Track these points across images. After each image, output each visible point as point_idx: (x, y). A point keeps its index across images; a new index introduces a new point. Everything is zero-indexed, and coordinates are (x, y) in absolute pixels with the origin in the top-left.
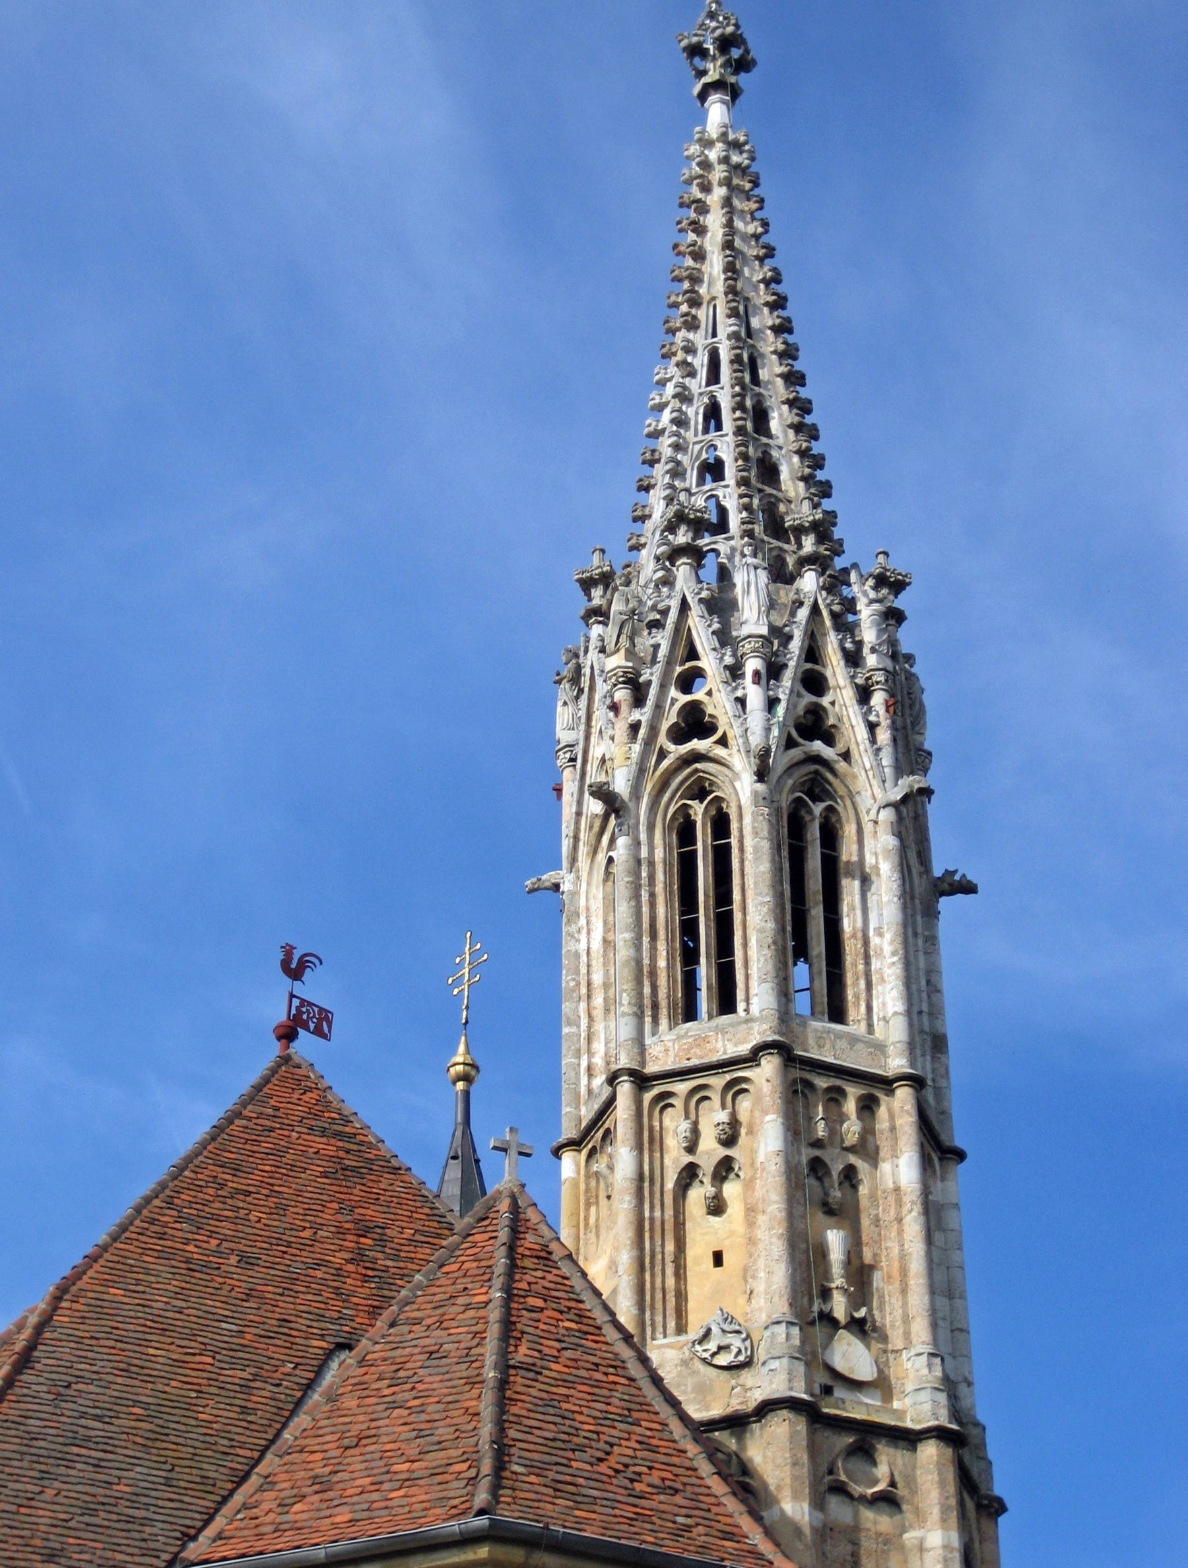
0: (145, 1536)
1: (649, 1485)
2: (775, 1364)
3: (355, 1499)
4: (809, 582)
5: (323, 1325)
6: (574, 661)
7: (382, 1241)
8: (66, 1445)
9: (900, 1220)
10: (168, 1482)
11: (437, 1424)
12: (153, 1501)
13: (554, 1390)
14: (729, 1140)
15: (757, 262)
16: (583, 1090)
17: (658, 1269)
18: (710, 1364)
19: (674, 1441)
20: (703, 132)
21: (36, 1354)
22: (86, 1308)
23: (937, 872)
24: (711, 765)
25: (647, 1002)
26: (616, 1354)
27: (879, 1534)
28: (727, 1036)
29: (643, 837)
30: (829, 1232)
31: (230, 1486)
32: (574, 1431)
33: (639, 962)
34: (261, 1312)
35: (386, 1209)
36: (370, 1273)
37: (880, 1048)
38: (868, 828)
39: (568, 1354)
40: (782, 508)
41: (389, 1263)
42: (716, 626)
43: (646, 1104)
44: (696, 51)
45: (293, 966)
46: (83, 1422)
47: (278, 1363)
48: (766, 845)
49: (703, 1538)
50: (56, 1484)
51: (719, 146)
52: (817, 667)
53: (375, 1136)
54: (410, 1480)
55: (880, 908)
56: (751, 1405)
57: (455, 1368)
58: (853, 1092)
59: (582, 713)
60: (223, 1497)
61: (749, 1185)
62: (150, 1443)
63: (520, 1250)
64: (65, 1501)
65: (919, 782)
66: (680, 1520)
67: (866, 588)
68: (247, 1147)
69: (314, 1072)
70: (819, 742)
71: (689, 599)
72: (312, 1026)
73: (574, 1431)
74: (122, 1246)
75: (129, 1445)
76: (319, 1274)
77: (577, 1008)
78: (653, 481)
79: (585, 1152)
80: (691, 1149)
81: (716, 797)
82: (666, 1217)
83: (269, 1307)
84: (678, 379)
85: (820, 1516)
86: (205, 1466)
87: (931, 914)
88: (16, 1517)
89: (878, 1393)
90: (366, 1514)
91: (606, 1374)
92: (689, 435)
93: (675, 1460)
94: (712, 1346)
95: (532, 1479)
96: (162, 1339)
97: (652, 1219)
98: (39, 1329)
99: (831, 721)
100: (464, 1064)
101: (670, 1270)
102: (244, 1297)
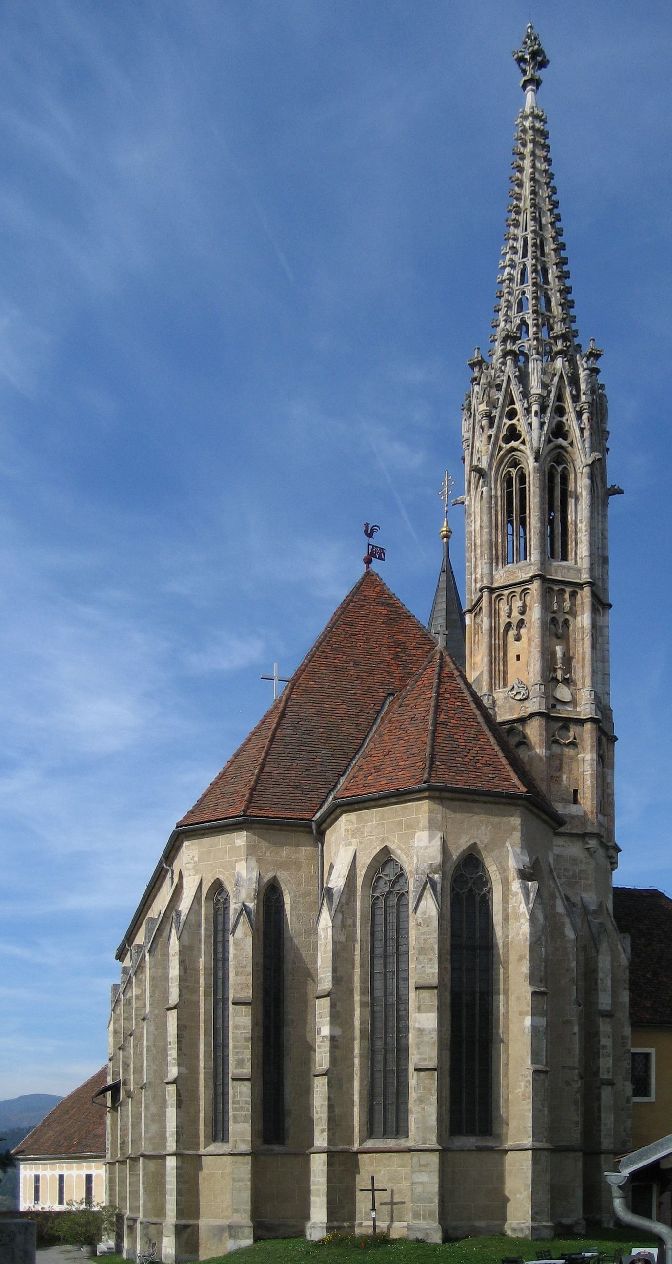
2: (535, 700)
3: (387, 775)
4: (559, 363)
7: (404, 649)
9: (583, 639)
10: (332, 756)
12: (328, 764)
13: (452, 731)
14: (522, 613)
17: (497, 663)
18: (514, 699)
19: (491, 746)
20: (524, 111)
21: (286, 711)
22: (302, 691)
23: (608, 486)
24: (519, 452)
25: (494, 557)
26: (474, 713)
27: (569, 756)
29: (493, 486)
30: (557, 647)
31: (353, 755)
32: (457, 746)
33: (491, 541)
35: (406, 635)
36: (400, 663)
37: (579, 571)
38: (579, 475)
41: (407, 658)
43: (493, 599)
45: (369, 532)
46: (303, 736)
48: (538, 490)
50: (296, 761)
51: (530, 119)
52: (561, 404)
53: (402, 603)
55: (582, 511)
56: (527, 715)
58: (568, 590)
59: (471, 426)
61: (529, 630)
62: (326, 742)
63: (443, 675)
64: (300, 767)
67: (583, 362)
68: (355, 615)
69: (378, 577)
70: (561, 439)
71: (511, 376)
72: (377, 556)
73: (457, 746)
74: (313, 664)
75: (319, 743)
76: (382, 666)
79: (474, 614)
80: (509, 617)
81: (521, 467)
87: (605, 504)
91: (470, 722)
92: (514, 285)
93: (491, 753)
94: (514, 692)
96: (328, 700)
98: (286, 702)
99: (566, 428)
100: (446, 531)
101: (501, 663)
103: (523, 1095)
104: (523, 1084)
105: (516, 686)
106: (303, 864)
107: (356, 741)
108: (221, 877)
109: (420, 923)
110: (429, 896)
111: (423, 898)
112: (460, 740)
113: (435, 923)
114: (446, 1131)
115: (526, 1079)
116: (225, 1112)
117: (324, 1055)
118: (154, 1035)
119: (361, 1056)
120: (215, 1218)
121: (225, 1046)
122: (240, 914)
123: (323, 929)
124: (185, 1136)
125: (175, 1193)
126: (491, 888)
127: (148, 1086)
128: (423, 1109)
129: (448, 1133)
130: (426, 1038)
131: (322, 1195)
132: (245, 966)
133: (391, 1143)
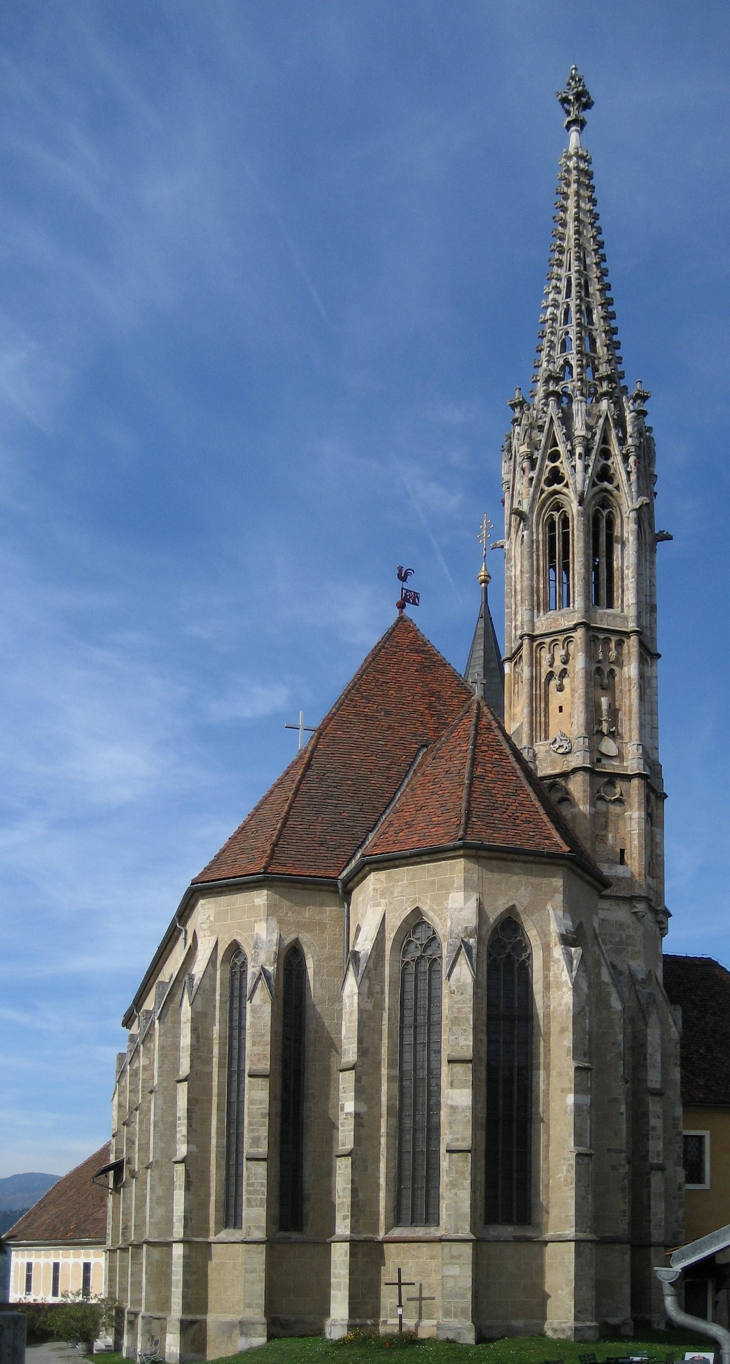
0: (354, 833)
1: (521, 821)
2: (578, 754)
3: (420, 832)
5: (416, 738)
6: (509, 441)
8: (324, 799)
9: (630, 691)
10: (361, 810)
11: (448, 802)
12: (356, 819)
14: (565, 662)
15: (590, 226)
16: (513, 636)
17: (538, 714)
18: (556, 752)
19: (532, 801)
20: (567, 151)
21: (312, 763)
22: (329, 741)
23: (657, 532)
24: (561, 495)
25: (535, 603)
27: (616, 814)
28: (565, 618)
29: (534, 530)
31: (383, 809)
32: (495, 802)
33: (532, 586)
34: (393, 735)
36: (434, 713)
37: (626, 619)
38: (625, 520)
39: (495, 769)
41: (442, 708)
42: (564, 431)
43: (534, 647)
45: (403, 575)
46: (330, 789)
47: (400, 756)
48: (582, 535)
49: (538, 840)
50: (322, 815)
51: (575, 159)
52: (607, 446)
53: (437, 651)
54: (437, 825)
55: (628, 557)
56: (570, 769)
57: (455, 778)
58: (614, 639)
59: (512, 468)
60: (381, 814)
61: (572, 680)
62: (354, 795)
63: (480, 726)
64: (325, 822)
65: (646, 500)
66: (530, 833)
67: (630, 404)
68: (387, 662)
71: (554, 417)
72: (411, 601)
73: (495, 802)
74: (341, 713)
75: (347, 797)
76: (415, 716)
77: (511, 601)
78: (543, 347)
79: (513, 663)
80: (551, 666)
82: (542, 693)
83: (396, 733)
85: (594, 809)
86: (374, 802)
87: (653, 550)
88: (309, 830)
89: (619, 760)
91: (509, 776)
92: (557, 326)
93: (531, 809)
94: (557, 746)
95: (479, 823)
97: (536, 694)
98: (312, 752)
99: (612, 472)
100: (485, 576)
101: (542, 715)
102: (387, 729)
103: (565, 1180)
104: (564, 1168)
105: (558, 739)
107: (386, 795)
108: (239, 939)
109: (454, 991)
110: (463, 962)
111: (457, 964)
112: (498, 796)
113: (470, 991)
114: (480, 1220)
115: (569, 1162)
116: (238, 1195)
117: (347, 1133)
121: (240, 1122)
122: (259, 979)
123: (348, 997)
125: (181, 1285)
126: (531, 954)
128: (456, 1194)
129: (482, 1222)
130: (459, 1117)
132: (263, 1036)
133: (420, 1232)
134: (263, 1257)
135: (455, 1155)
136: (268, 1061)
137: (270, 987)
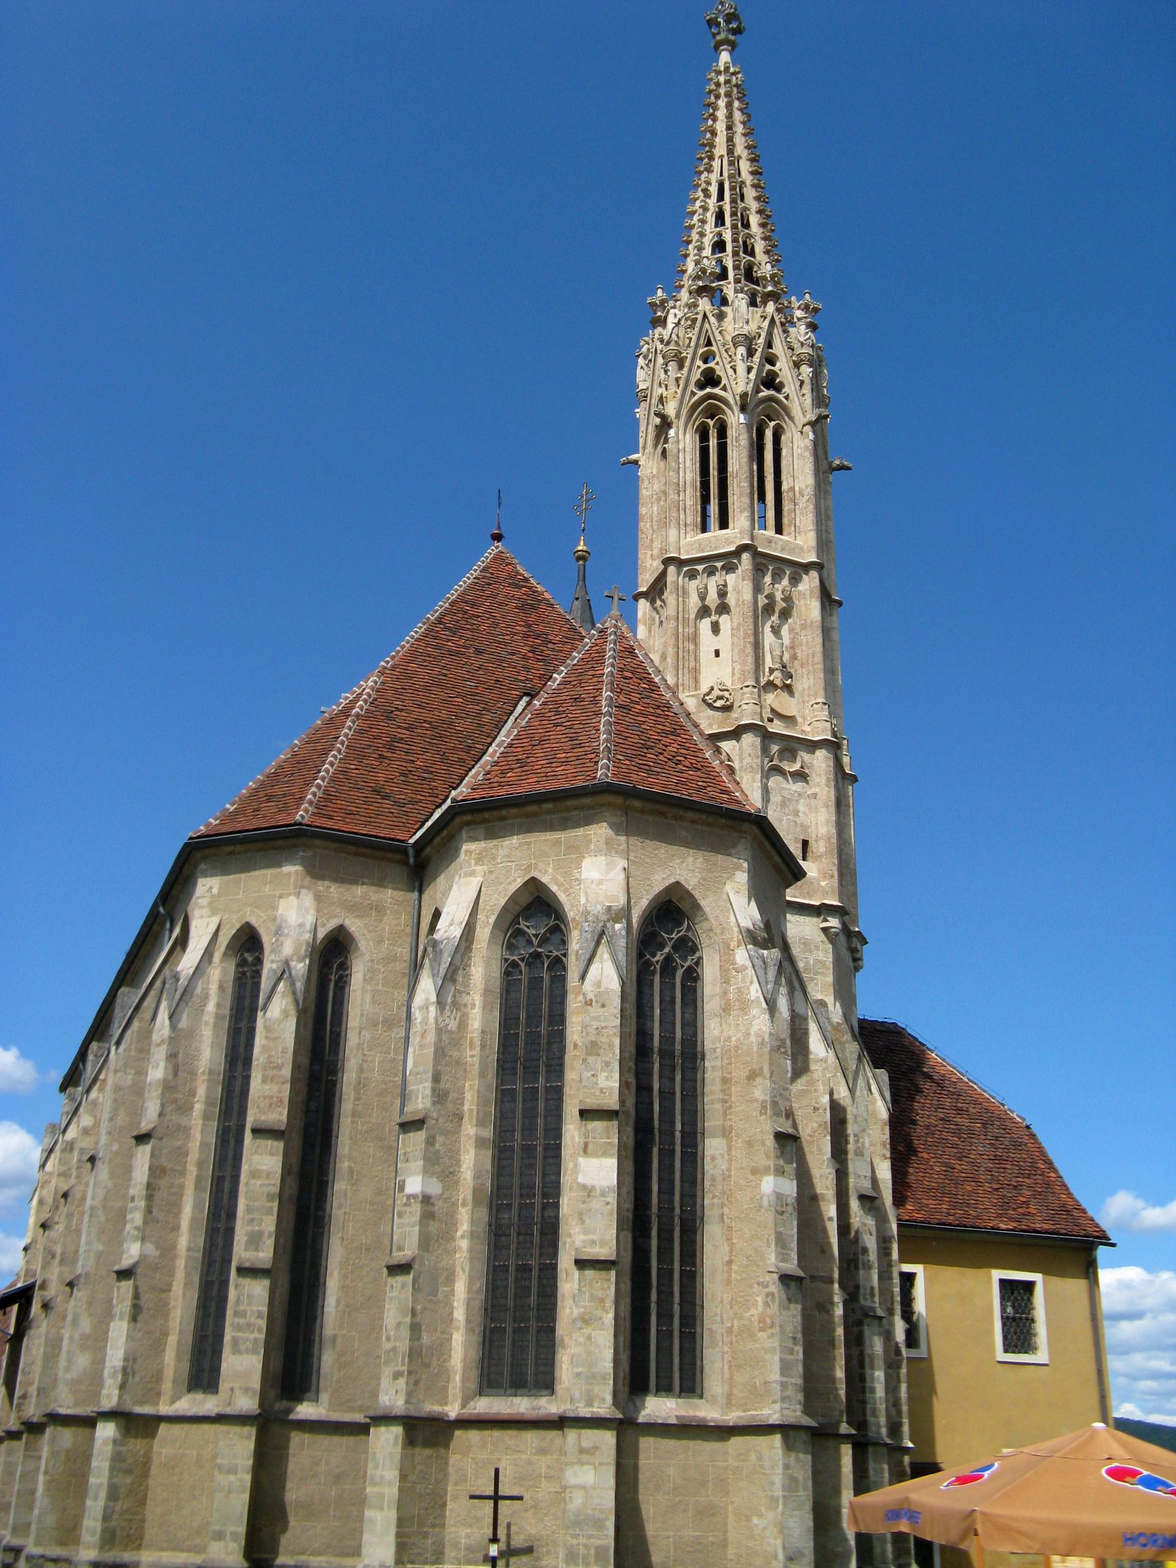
39: (645, 700)
40: (755, 268)
44: (712, 23)
46: (399, 730)
54: (566, 762)
84: (702, 198)
90: (545, 778)
103: (762, 1320)
104: (760, 1299)
105: (716, 688)
106: (388, 911)
107: (478, 746)
108: (254, 922)
109: (591, 1000)
110: (606, 956)
111: (597, 959)
112: (651, 732)
113: (617, 1001)
114: (624, 1385)
115: (767, 1290)
116: (219, 1337)
117: (407, 1229)
118: (106, 1187)
119: (473, 1235)
120: (173, 1550)
121: (232, 1215)
122: (280, 979)
123: (421, 1008)
124: (137, 1378)
125: (103, 1494)
126: (700, 958)
127: (83, 1280)
128: (589, 1337)
129: (627, 1389)
130: (596, 1204)
131: (388, 1507)
132: (279, 1067)
133: (521, 1405)
134: (251, 1445)
135: (589, 1273)
136: (284, 1108)
137: (294, 993)
